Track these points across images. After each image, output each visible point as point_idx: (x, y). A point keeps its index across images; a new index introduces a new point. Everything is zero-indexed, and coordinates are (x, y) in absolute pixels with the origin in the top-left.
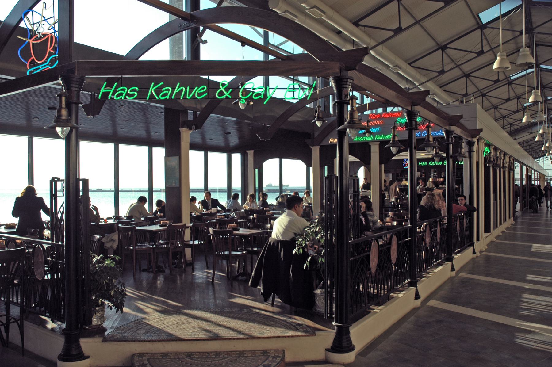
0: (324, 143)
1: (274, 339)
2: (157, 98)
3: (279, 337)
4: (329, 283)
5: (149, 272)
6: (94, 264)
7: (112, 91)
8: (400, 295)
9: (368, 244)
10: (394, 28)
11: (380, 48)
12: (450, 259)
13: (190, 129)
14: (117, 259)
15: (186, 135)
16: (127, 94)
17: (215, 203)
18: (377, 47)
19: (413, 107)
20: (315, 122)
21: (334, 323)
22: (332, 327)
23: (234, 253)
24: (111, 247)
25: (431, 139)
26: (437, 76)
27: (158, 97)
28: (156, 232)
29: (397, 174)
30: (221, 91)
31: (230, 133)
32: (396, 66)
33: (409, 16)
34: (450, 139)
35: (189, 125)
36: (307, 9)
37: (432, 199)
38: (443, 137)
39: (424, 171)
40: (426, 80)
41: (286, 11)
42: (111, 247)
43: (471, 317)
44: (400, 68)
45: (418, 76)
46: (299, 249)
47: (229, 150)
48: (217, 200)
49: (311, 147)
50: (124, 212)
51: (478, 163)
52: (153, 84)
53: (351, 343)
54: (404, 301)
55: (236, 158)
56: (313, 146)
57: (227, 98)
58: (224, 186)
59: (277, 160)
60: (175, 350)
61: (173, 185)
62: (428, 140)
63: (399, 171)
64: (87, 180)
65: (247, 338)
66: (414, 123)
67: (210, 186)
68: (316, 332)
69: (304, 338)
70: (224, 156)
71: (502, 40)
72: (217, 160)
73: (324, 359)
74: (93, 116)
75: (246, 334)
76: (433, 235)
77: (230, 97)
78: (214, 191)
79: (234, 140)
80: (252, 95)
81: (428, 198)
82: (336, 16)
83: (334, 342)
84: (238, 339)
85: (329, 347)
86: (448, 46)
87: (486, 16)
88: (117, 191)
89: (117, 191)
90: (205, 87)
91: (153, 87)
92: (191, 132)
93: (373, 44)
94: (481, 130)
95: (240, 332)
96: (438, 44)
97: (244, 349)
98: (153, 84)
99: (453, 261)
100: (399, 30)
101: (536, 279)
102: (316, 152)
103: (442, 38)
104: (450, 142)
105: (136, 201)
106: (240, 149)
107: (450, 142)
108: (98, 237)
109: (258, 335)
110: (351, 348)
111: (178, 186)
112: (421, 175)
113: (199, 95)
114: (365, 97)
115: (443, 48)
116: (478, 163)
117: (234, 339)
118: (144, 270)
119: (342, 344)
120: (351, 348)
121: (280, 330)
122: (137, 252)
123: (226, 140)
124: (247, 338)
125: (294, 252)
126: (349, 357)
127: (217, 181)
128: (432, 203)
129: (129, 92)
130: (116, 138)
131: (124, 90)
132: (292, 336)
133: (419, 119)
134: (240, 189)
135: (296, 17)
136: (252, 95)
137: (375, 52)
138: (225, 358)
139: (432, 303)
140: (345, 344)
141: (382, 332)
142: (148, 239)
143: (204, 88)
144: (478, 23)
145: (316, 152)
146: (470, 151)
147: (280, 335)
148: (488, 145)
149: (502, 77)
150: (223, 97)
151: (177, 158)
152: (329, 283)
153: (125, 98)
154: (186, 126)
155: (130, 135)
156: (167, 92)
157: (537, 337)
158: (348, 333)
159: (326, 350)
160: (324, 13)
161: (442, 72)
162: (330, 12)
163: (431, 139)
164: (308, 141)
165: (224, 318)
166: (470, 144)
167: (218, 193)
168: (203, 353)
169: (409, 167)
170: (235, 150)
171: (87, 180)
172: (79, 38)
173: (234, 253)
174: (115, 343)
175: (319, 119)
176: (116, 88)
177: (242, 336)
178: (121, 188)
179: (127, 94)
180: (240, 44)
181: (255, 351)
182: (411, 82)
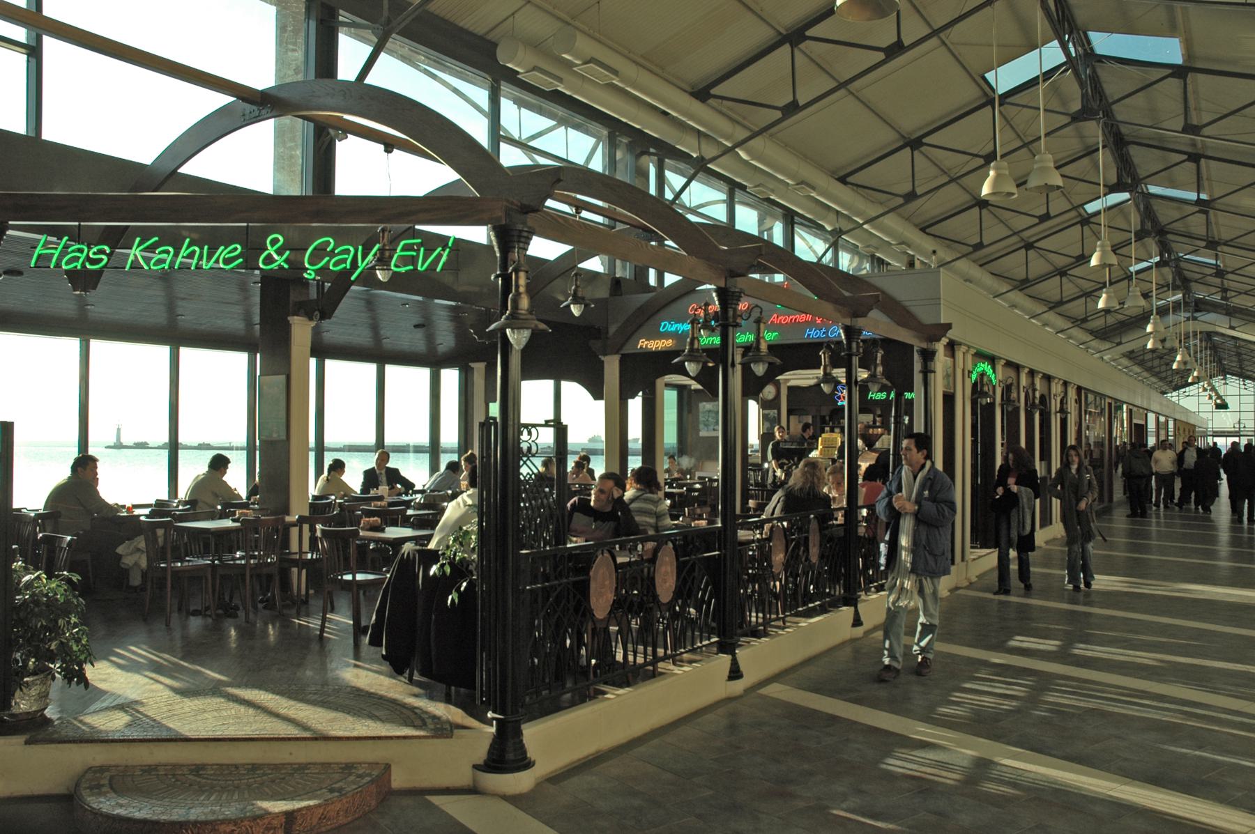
0: (627, 350)
1: (370, 742)
2: (146, 267)
3: (380, 738)
4: (568, 642)
5: (205, 616)
6: (266, 624)
7: (57, 253)
8: (677, 670)
9: (583, 561)
10: (781, 103)
11: (757, 143)
12: (851, 601)
13: (311, 319)
14: (74, 579)
15: (301, 330)
16: (88, 259)
17: (394, 476)
18: (752, 143)
19: (731, 281)
20: (568, 306)
21: (490, 715)
22: (488, 722)
23: (359, 577)
24: (136, 564)
25: (763, 347)
26: (901, 206)
27: (148, 264)
28: (227, 531)
29: (823, 418)
30: (270, 255)
31: (416, 326)
32: (802, 183)
33: (825, 76)
34: (854, 345)
35: (307, 310)
36: (577, 65)
37: (813, 475)
38: (839, 343)
39: (879, 412)
40: (881, 211)
41: (535, 68)
42: (136, 564)
43: (833, 719)
44: (813, 188)
45: (860, 203)
46: (443, 566)
47: (434, 361)
48: (396, 471)
49: (602, 358)
50: (183, 492)
51: (949, 399)
52: (138, 239)
53: (525, 752)
54: (693, 682)
55: (451, 378)
56: (605, 354)
57: (281, 267)
58: (424, 439)
59: (549, 384)
60: (173, 760)
61: (275, 435)
62: (758, 349)
63: (825, 411)
64: (12, 423)
65: (316, 739)
66: (731, 313)
67: (389, 440)
68: (456, 731)
69: (430, 741)
70: (424, 374)
71: (1046, 127)
72: (408, 382)
73: (471, 784)
74: (85, 291)
75: (314, 731)
76: (797, 547)
77: (286, 266)
78: (402, 449)
79: (446, 340)
80: (329, 262)
81: (804, 474)
82: (645, 78)
83: (490, 752)
84: (297, 739)
85: (481, 762)
86: (924, 140)
87: (1006, 78)
88: (174, 447)
89: (174, 447)
90: (281, 238)
91: (140, 244)
92: (313, 324)
93: (742, 134)
94: (948, 326)
95: (305, 728)
96: (903, 137)
97: (309, 760)
98: (138, 239)
99: (859, 606)
100: (792, 108)
101: (1025, 645)
102: (612, 367)
103: (911, 123)
104: (854, 350)
105: (205, 469)
106: (460, 358)
107: (854, 350)
108: (69, 538)
109: (340, 733)
110: (524, 763)
111: (284, 438)
112: (875, 421)
113: (227, 261)
114: (618, 263)
115: (915, 144)
116: (949, 399)
117: (290, 739)
118: (196, 613)
119: (506, 755)
120: (524, 763)
121: (388, 726)
122: (176, 572)
123: (430, 339)
124: (316, 739)
125: (431, 573)
126: (520, 782)
127: (408, 426)
128: (813, 483)
129: (91, 255)
130: (175, 335)
131: (81, 251)
132: (405, 737)
133: (743, 306)
134: (457, 446)
135: (560, 80)
136: (329, 262)
137: (748, 152)
138: (264, 774)
139: (776, 691)
140: (510, 756)
141: (624, 741)
142: (353, 563)
143: (236, 249)
144: (986, 94)
145: (612, 367)
146: (926, 372)
147: (383, 734)
148: (981, 356)
149: (1058, 205)
150: (274, 266)
151: (282, 378)
152: (568, 642)
153: (83, 265)
154: (302, 311)
155: (203, 327)
156: (165, 256)
157: (931, 755)
158: (519, 733)
159: (475, 767)
160: (616, 72)
161: (911, 196)
162: (629, 69)
163: (763, 347)
164: (596, 345)
165: (292, 703)
166: (928, 356)
167: (411, 455)
168: (228, 765)
169: (845, 403)
170: (447, 361)
171: (12, 423)
172: (47, 135)
173: (359, 577)
174: (53, 746)
175: (576, 300)
176: (66, 247)
177: (293, 732)
178: (182, 439)
179: (88, 259)
180: (382, 147)
181: (330, 764)
182: (849, 218)
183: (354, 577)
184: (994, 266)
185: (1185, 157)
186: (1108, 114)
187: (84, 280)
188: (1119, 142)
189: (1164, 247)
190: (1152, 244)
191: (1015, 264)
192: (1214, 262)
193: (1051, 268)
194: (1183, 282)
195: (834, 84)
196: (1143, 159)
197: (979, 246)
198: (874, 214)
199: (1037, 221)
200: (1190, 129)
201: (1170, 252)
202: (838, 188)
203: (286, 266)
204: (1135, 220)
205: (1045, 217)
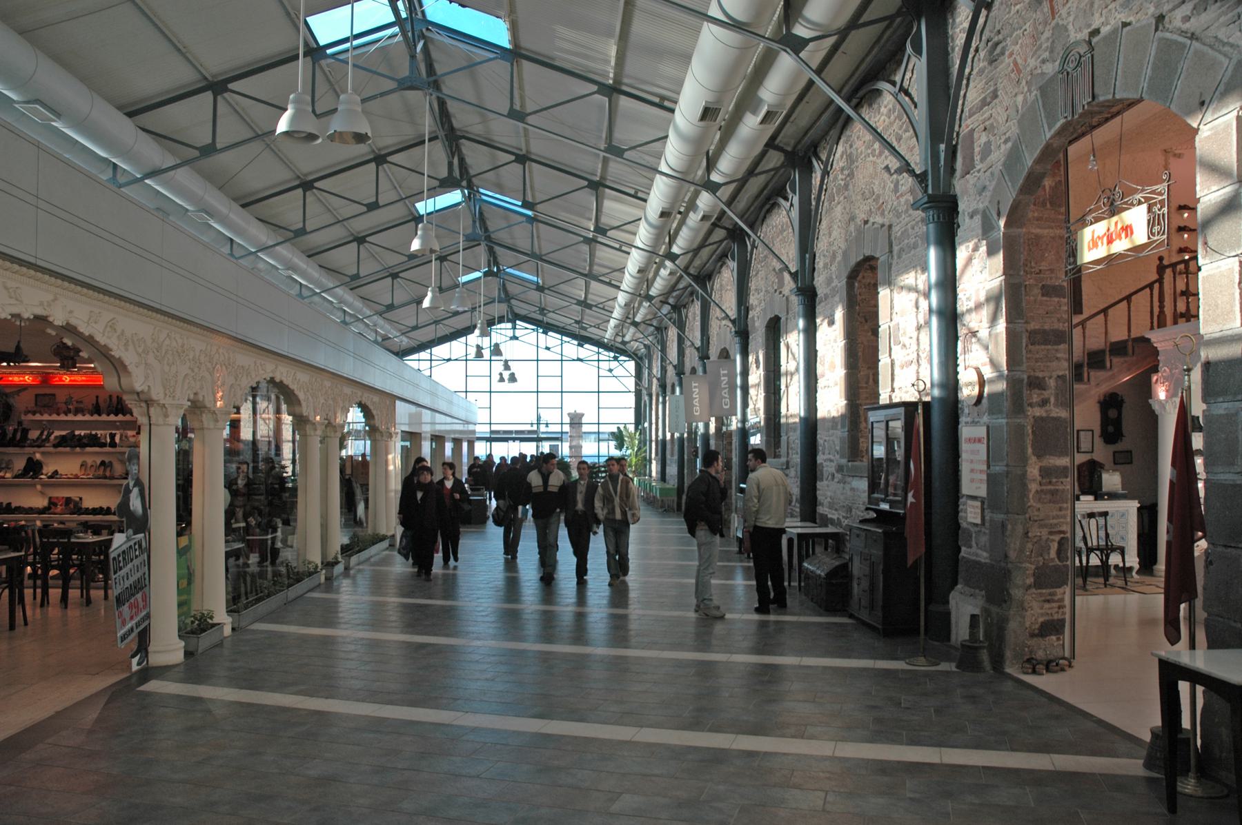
86: (316, 185)
96: (206, 79)
103: (216, 63)
115: (307, 186)
183: (1199, 452)
184: (148, 119)
185: (513, 158)
186: (436, 85)
187: (1050, 594)
188: (452, 137)
189: (493, 259)
190: (481, 252)
191: (345, 257)
192: (535, 279)
193: (287, 175)
194: (507, 297)
195: (253, 135)
196: (476, 157)
197: (302, 232)
198: (271, 243)
199: (365, 209)
200: (518, 115)
201: (497, 263)
202: (125, 128)
203: (408, 444)
204: (464, 225)
205: (373, 207)
